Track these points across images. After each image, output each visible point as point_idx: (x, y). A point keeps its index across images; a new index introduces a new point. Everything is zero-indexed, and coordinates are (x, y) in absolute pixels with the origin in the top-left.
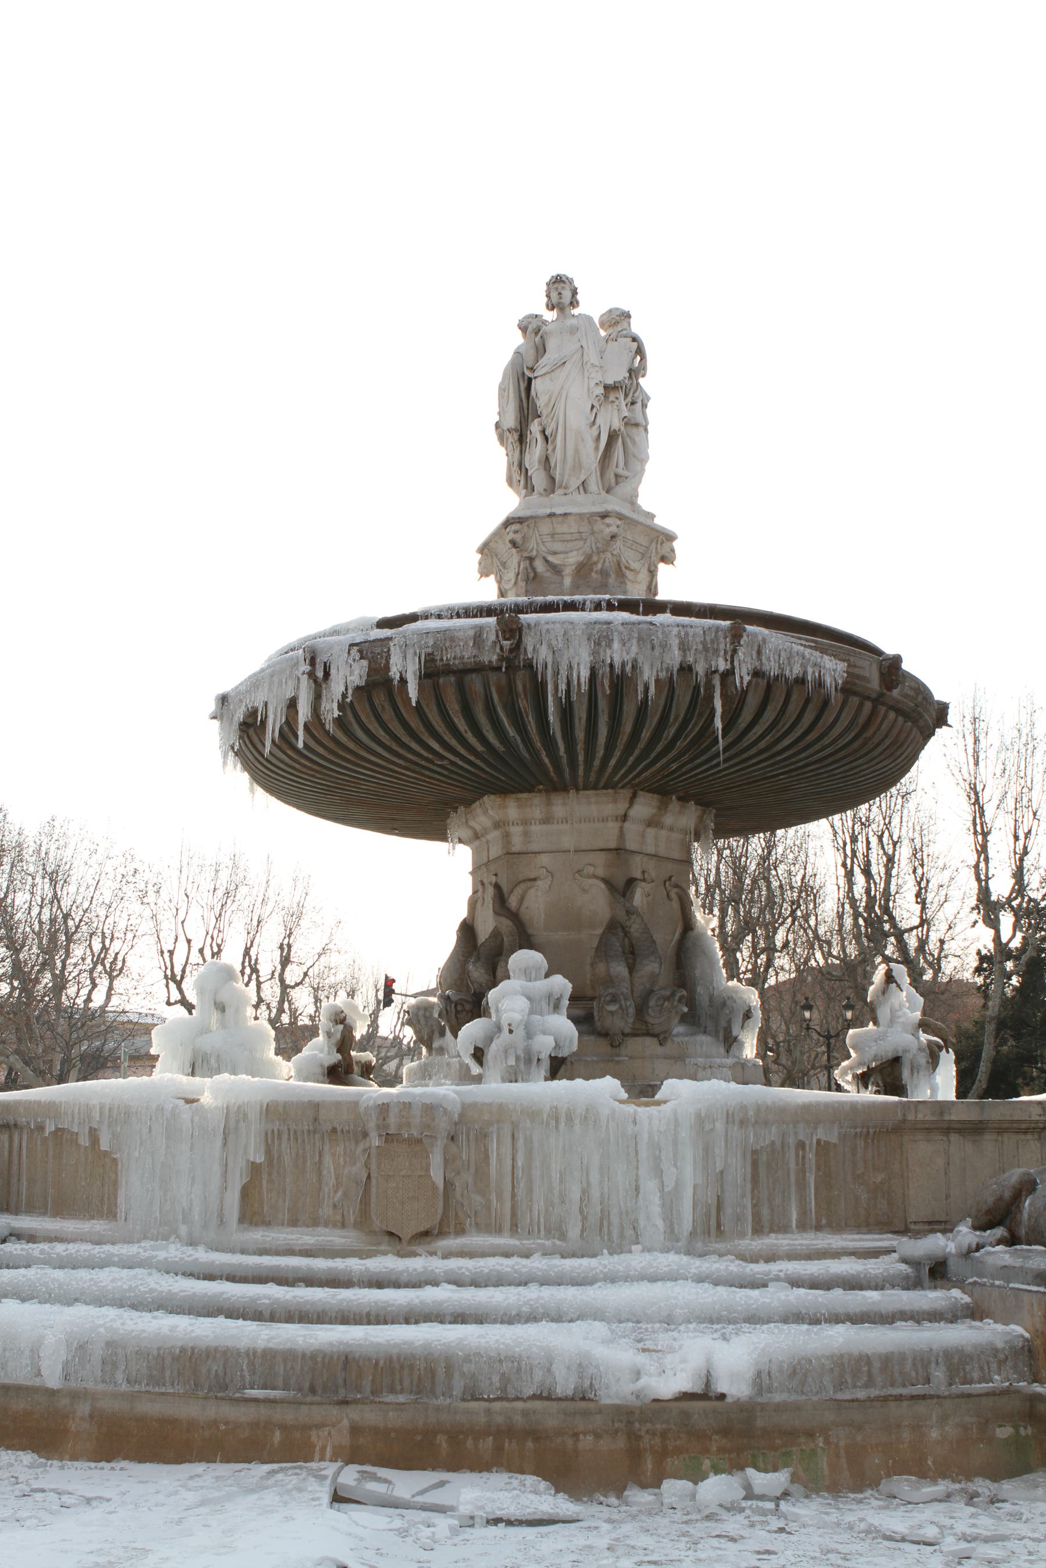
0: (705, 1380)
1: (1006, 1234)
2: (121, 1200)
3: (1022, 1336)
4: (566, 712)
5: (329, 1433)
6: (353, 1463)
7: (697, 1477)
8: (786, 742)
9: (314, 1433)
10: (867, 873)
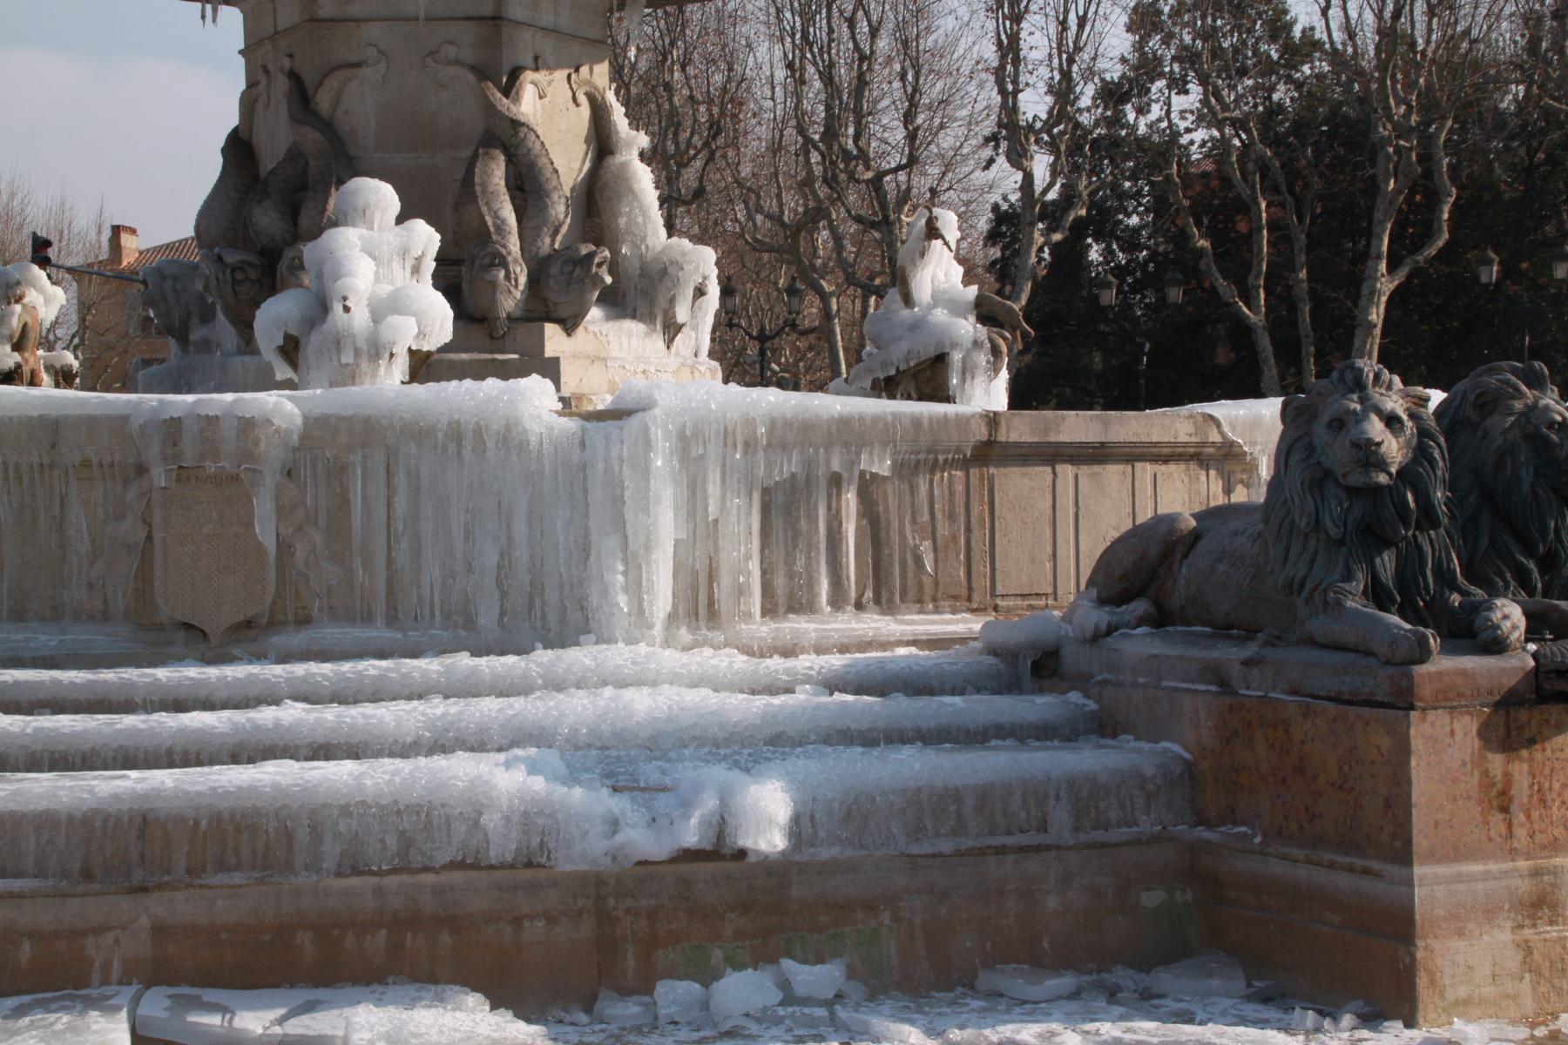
0: (717, 829)
1: (1152, 610)
3: (1181, 757)
5: (117, 940)
6: (159, 983)
7: (708, 977)
9: (90, 941)
10: (828, 77)
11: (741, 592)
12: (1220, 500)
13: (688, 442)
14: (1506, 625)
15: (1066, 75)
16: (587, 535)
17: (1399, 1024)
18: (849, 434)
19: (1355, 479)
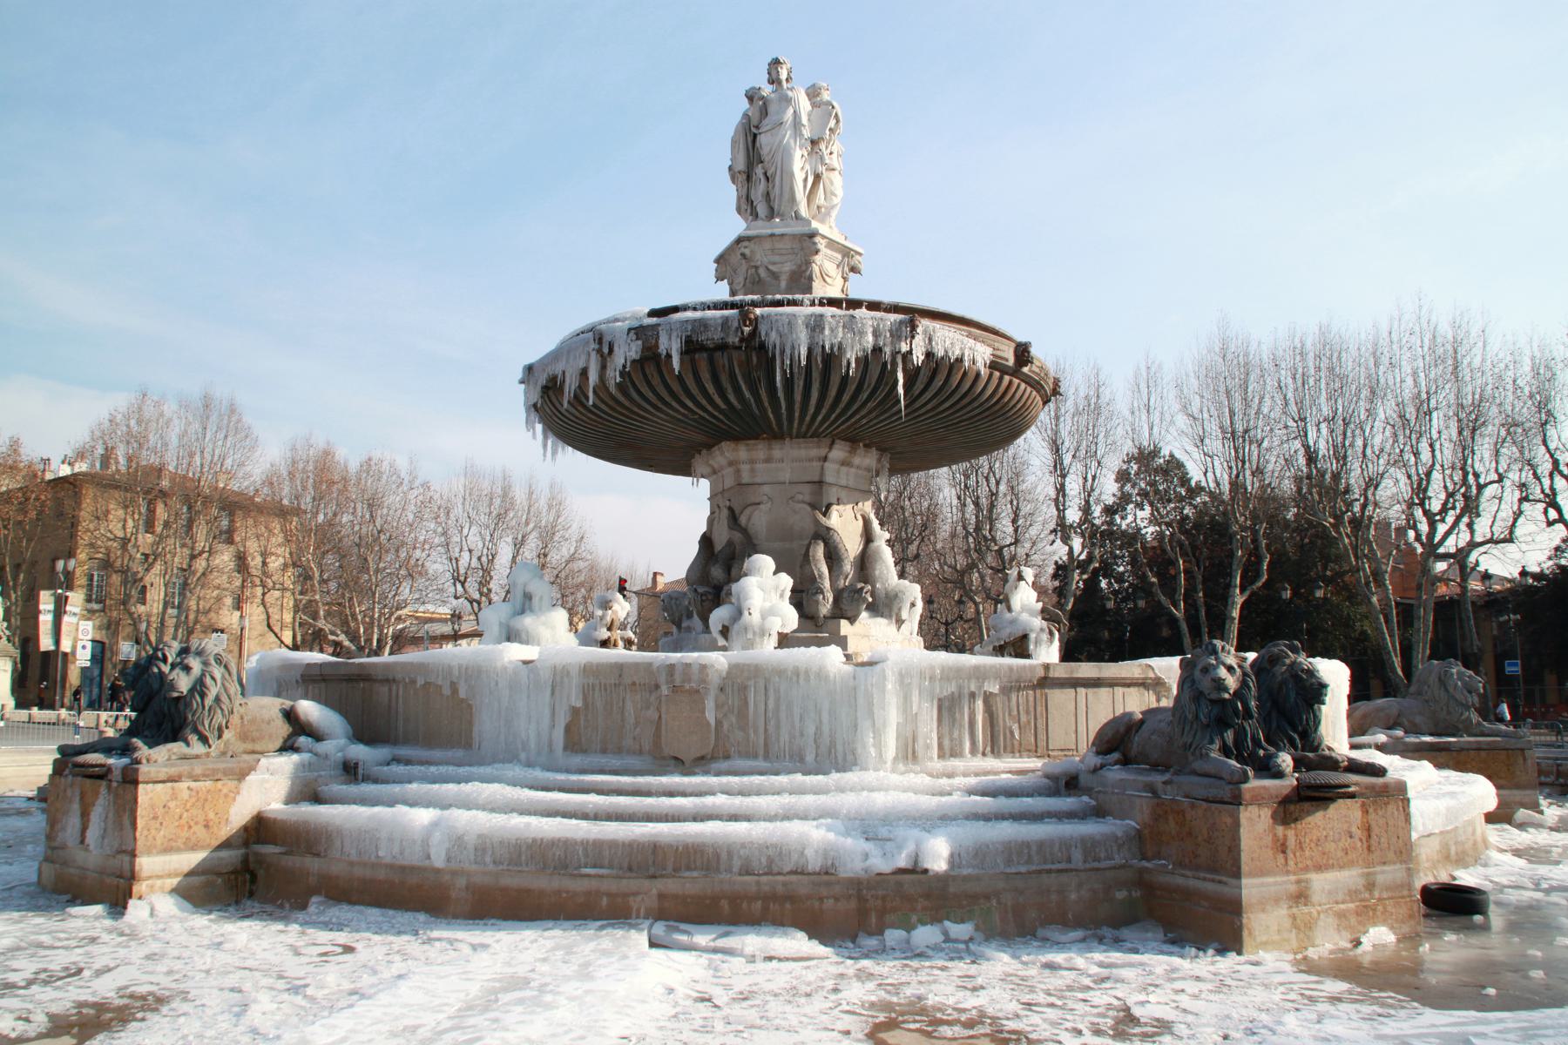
2: (475, 734)
4: (789, 383)
7: (909, 928)
8: (947, 405)
9: (631, 898)
10: (976, 504)
11: (928, 747)
12: (1154, 705)
13: (903, 677)
14: (1284, 765)
15: (1087, 502)
16: (856, 719)
17: (1234, 954)
18: (980, 674)
19: (1214, 696)
